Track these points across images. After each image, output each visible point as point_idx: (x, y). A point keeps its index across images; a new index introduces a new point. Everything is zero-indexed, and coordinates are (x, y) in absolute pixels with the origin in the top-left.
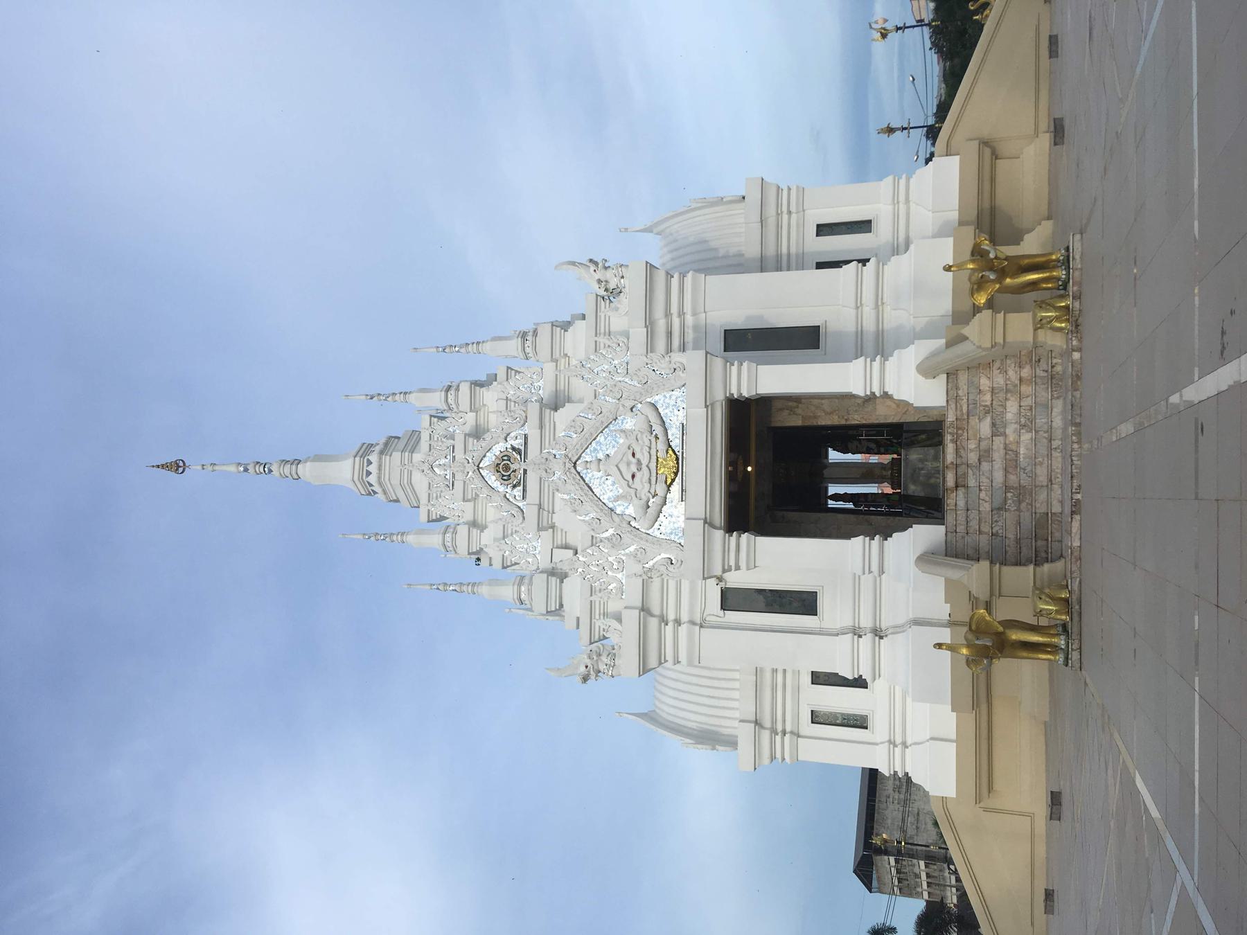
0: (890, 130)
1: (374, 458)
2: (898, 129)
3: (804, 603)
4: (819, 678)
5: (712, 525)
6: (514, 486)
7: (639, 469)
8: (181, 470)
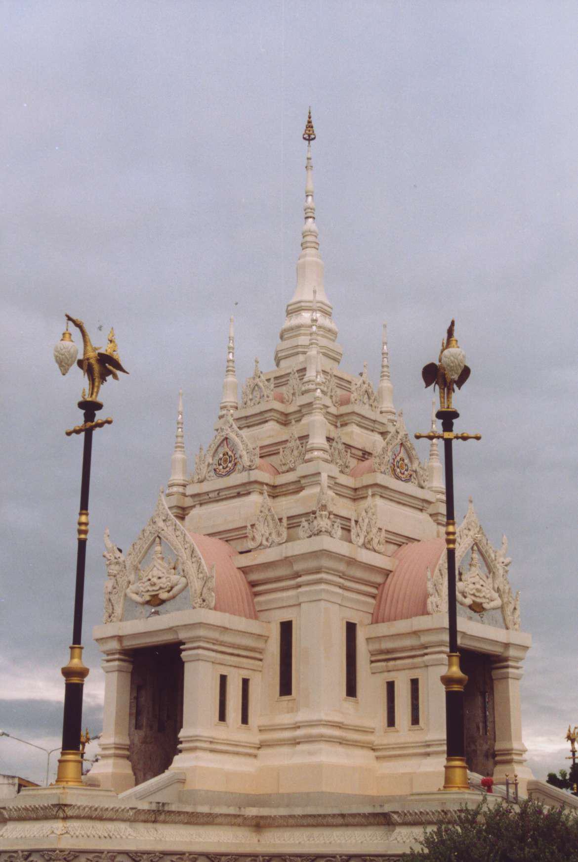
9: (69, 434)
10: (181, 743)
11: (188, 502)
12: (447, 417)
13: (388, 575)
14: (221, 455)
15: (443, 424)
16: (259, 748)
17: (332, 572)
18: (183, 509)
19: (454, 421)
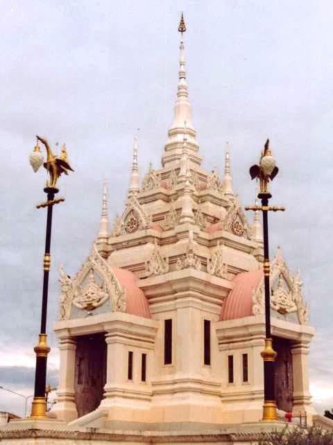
9: (38, 207)
10: (105, 392)
11: (110, 248)
12: (265, 198)
13: (229, 292)
14: (130, 220)
16: (152, 396)
18: (107, 252)
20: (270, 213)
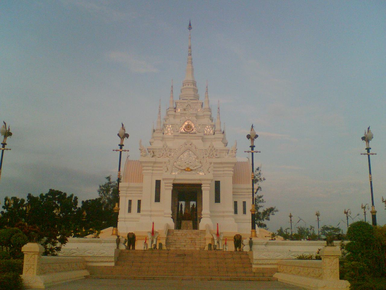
0: (291, 216)
1: (192, 86)
2: (291, 219)
3: (157, 199)
4: (139, 202)
5: (174, 180)
6: (184, 129)
7: (187, 164)
8: (189, 28)
12: (252, 147)
15: (252, 149)
17: (134, 192)
19: (254, 148)
20: (371, 156)
